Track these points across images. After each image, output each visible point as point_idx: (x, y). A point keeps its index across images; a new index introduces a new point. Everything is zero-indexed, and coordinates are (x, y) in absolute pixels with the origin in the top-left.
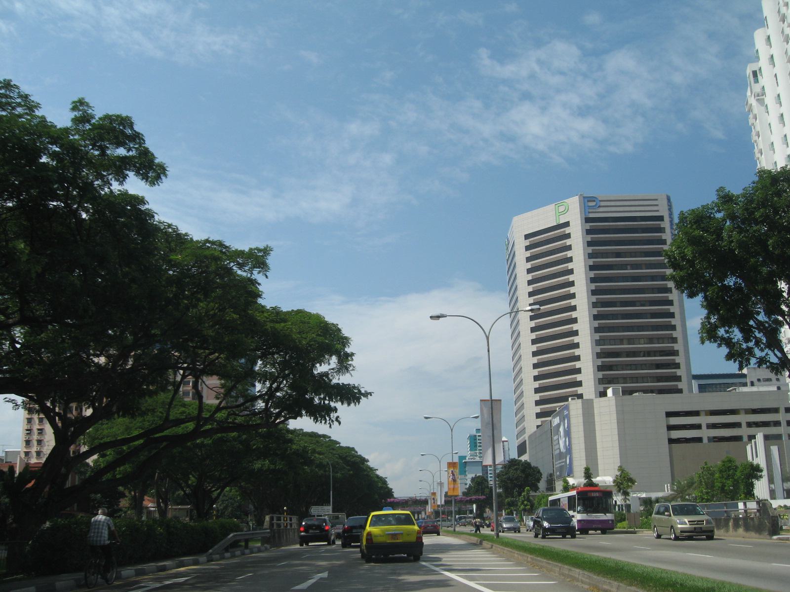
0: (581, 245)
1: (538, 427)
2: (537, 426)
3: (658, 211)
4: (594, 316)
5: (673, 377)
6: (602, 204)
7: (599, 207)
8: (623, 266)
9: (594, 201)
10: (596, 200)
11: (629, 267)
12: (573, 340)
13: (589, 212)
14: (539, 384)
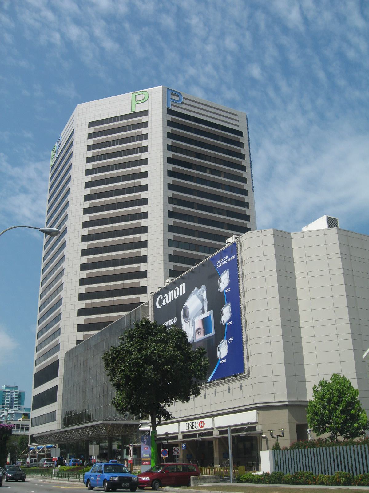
0: (161, 173)
1: (78, 342)
2: (77, 341)
3: (238, 126)
4: (169, 212)
5: (236, 141)
6: (186, 101)
7: (183, 103)
8: (203, 169)
9: (178, 96)
10: (179, 95)
11: (208, 171)
12: (140, 237)
13: (172, 105)
14: (90, 217)
